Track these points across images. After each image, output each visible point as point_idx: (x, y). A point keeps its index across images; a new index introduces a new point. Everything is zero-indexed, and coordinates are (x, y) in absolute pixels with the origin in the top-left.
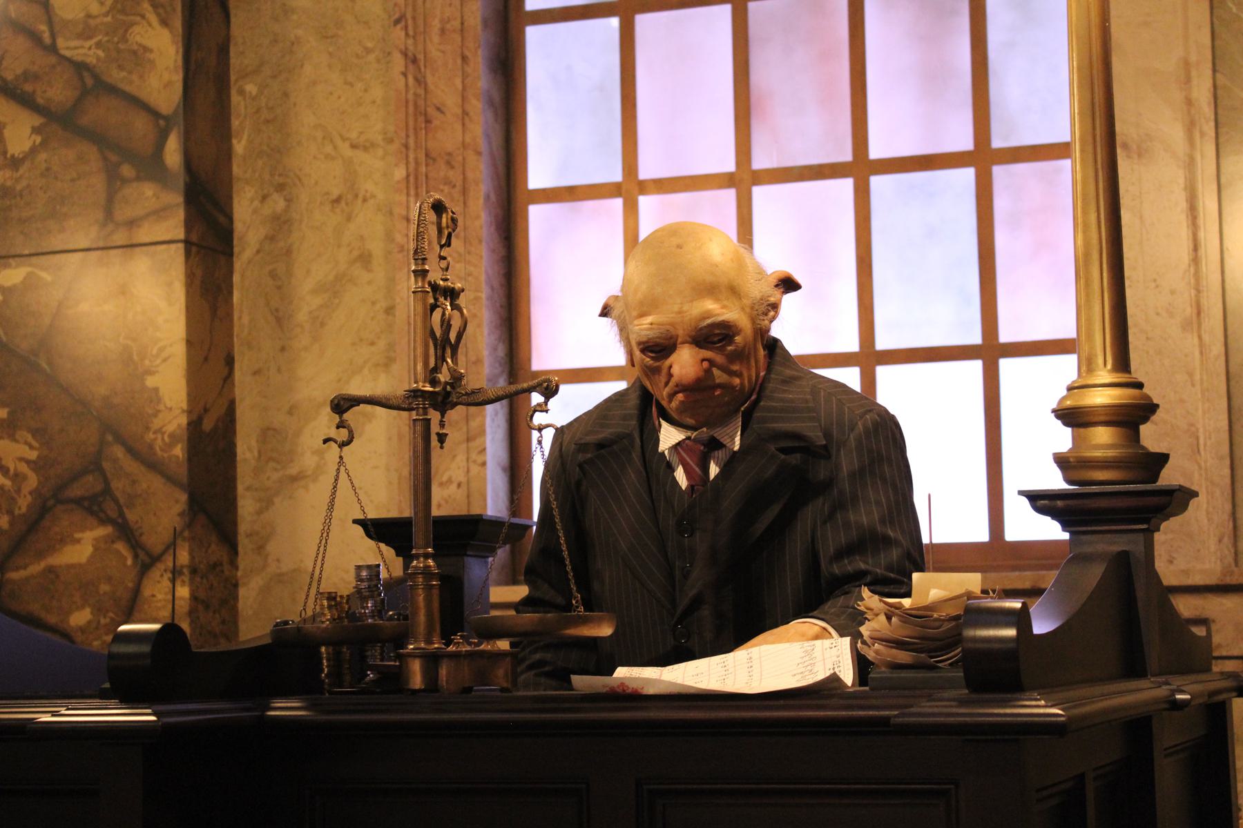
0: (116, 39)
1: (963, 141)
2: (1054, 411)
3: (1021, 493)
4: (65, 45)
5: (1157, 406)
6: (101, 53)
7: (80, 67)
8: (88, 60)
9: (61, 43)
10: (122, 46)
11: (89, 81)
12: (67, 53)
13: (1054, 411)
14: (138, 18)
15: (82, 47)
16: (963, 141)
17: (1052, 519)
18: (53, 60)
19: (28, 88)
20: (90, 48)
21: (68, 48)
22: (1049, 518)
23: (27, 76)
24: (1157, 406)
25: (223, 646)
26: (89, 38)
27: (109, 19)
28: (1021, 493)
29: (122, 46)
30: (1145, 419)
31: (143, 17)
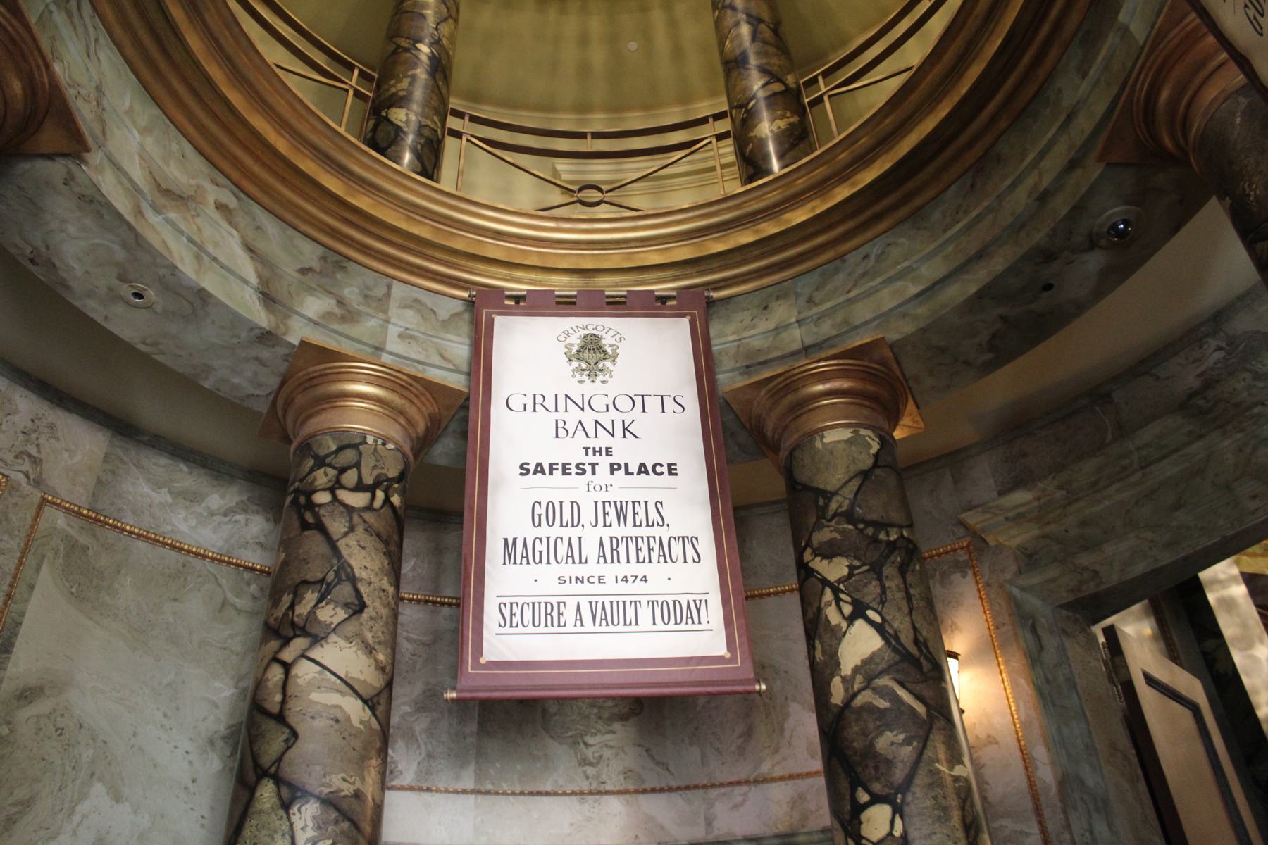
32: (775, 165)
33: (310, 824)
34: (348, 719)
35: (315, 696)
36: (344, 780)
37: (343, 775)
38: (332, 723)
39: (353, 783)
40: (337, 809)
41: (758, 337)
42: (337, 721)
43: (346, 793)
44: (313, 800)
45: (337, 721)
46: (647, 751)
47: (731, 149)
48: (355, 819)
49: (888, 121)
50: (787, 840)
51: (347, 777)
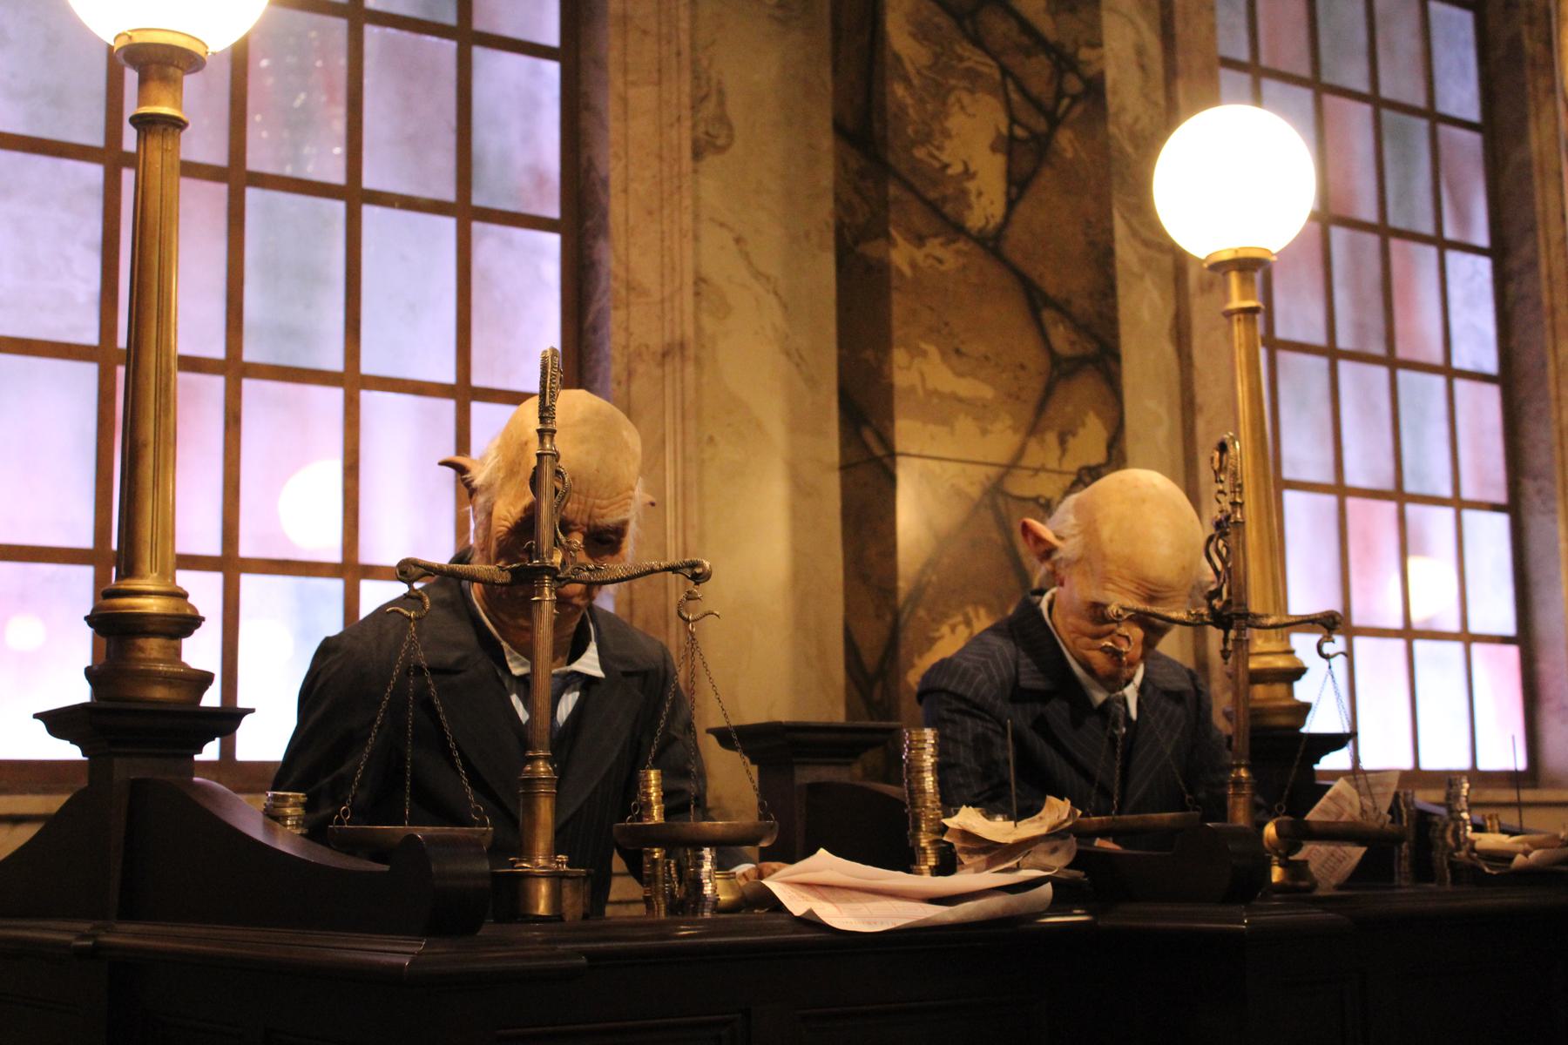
0: (945, 59)
1: (252, 353)
2: (87, 618)
3: (36, 716)
4: (989, 69)
5: (203, 619)
6: (959, 50)
7: (978, 42)
8: (970, 47)
9: (997, 76)
10: (938, 49)
11: (967, 23)
12: (989, 61)
13: (87, 618)
14: (925, 72)
15: (977, 62)
16: (250, 354)
17: (71, 743)
18: (1004, 59)
19: (1025, 40)
20: (969, 59)
21: (991, 66)
22: (68, 742)
23: (1028, 54)
24: (203, 619)
25: (1285, 703)
26: (968, 70)
27: (952, 82)
28: (36, 716)
29: (938, 49)
30: (188, 633)
31: (919, 72)
32: (662, 914)
33: (973, 198)
34: (943, 354)
35: (987, 392)
36: (940, 261)
37: (943, 268)
38: (964, 349)
39: (927, 256)
40: (944, 218)
41: (546, 782)
42: (958, 351)
43: (937, 241)
44: (974, 232)
45: (958, 351)
46: (738, 240)
47: (1445, 754)
48: (1342, 213)
49: (1167, 815)
50: (1563, 146)
51: (937, 265)
